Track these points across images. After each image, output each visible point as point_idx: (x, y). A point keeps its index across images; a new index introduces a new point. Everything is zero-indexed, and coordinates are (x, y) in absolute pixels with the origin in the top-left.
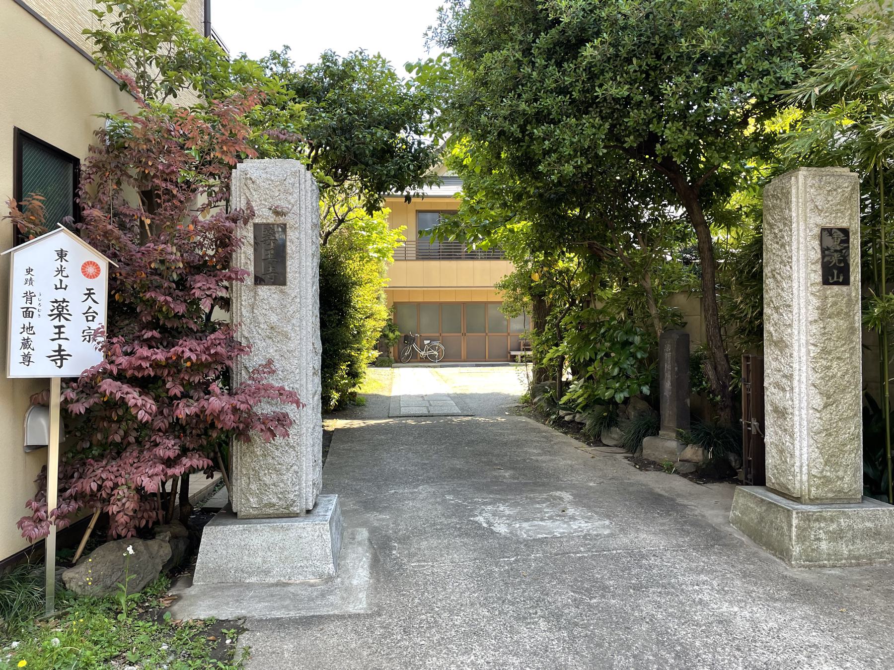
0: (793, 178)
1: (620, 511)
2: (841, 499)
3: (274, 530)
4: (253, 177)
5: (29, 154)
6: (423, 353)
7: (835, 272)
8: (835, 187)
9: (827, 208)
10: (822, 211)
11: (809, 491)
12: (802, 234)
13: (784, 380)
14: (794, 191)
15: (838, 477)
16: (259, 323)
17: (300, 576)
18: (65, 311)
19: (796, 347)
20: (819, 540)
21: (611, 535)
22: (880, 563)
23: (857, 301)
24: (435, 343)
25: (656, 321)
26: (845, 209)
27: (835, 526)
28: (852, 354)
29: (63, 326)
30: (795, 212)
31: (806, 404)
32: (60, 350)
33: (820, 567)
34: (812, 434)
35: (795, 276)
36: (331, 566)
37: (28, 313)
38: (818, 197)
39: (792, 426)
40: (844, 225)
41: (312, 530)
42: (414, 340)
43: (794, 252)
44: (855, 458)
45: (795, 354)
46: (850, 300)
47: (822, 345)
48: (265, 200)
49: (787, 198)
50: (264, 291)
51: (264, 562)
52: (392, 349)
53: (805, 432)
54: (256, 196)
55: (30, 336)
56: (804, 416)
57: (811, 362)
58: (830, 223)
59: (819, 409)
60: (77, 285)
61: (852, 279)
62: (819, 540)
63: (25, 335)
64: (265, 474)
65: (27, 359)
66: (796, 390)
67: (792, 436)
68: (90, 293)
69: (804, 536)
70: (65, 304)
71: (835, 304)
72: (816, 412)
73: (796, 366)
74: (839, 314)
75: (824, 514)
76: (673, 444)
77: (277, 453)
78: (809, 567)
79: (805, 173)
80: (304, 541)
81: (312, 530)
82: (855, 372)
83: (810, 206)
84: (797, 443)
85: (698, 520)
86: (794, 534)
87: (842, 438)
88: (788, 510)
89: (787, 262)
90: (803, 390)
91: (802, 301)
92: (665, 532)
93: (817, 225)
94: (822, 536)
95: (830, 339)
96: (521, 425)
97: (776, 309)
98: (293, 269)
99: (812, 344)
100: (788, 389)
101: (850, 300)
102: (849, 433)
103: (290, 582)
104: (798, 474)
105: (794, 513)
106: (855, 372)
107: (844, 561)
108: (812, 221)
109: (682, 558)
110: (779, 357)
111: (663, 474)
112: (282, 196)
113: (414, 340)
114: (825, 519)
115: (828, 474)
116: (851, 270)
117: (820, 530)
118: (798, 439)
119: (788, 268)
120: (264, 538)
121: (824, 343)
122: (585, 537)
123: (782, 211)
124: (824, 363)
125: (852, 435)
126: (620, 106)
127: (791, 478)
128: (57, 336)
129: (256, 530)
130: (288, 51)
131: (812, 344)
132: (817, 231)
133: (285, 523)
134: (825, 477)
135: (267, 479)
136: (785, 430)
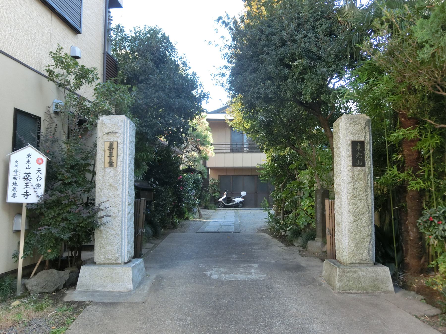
2: (362, 263)
3: (109, 269)
5: (19, 117)
7: (359, 161)
9: (354, 132)
16: (106, 183)
18: (29, 177)
29: (28, 183)
32: (27, 192)
36: (132, 285)
37: (15, 178)
38: (350, 128)
44: (369, 245)
55: (16, 187)
60: (34, 166)
61: (366, 164)
63: (14, 186)
64: (107, 246)
65: (14, 195)
68: (39, 170)
70: (29, 175)
77: (112, 238)
86: (337, 278)
93: (350, 140)
97: (336, 177)
114: (352, 272)
116: (366, 160)
124: (354, 201)
125: (367, 234)
128: (26, 187)
129: (102, 269)
132: (350, 142)
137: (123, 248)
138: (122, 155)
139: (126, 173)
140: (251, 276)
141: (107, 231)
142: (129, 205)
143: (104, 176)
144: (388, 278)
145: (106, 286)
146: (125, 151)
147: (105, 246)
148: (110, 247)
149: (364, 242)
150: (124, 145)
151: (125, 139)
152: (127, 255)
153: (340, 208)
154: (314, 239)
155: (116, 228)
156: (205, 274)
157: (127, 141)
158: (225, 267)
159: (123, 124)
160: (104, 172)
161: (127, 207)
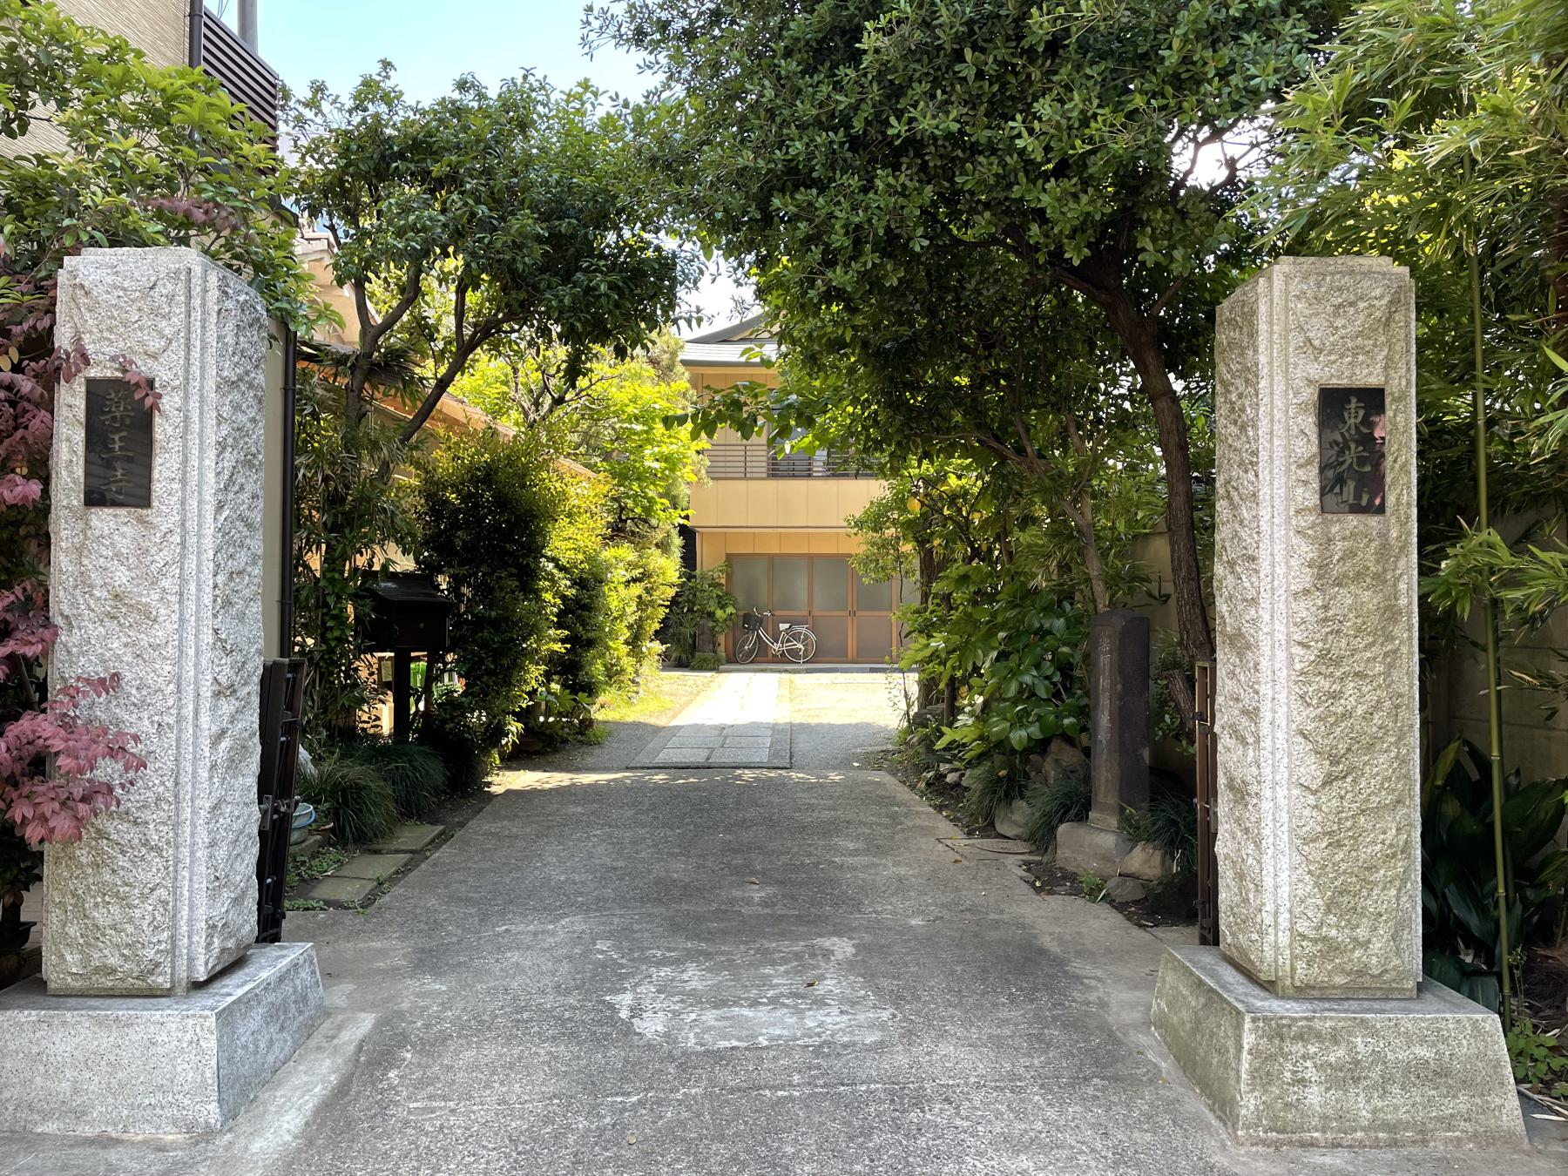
0: (1261, 280)
1: (932, 988)
3: (100, 1024)
4: (86, 284)
6: (776, 647)
8: (1352, 298)
10: (1321, 351)
11: (1293, 969)
12: (1279, 403)
13: (1245, 721)
14: (1263, 309)
15: (1355, 940)
17: (146, 1126)
19: (1265, 648)
20: (1303, 1082)
21: (879, 1047)
22: (1447, 1141)
23: (1403, 548)
24: (798, 629)
25: (1099, 587)
26: (1375, 345)
27: (1341, 1053)
28: (1390, 666)
30: (1264, 356)
31: (1286, 775)
33: (1303, 1144)
34: (1299, 842)
35: (1265, 492)
36: (213, 1107)
38: (1314, 320)
39: (1259, 821)
40: (1374, 380)
41: (178, 1029)
42: (760, 622)
43: (1263, 441)
44: (1398, 898)
45: (1264, 664)
46: (1385, 546)
47: (1320, 645)
48: (110, 330)
49: (1251, 324)
50: (104, 519)
51: (76, 1091)
52: (721, 639)
53: (1285, 837)
54: (90, 322)
56: (1282, 802)
57: (1296, 682)
58: (1339, 378)
59: (1314, 787)
62: (1303, 1082)
64: (96, 905)
66: (1267, 743)
67: (1258, 845)
69: (1268, 1073)
71: (1349, 554)
72: (1307, 794)
73: (1265, 689)
74: (1359, 576)
75: (1317, 1024)
76: (1108, 841)
78: (1277, 1145)
79: (1286, 268)
80: (160, 1050)
81: (178, 1029)
82: (1397, 707)
83: (1296, 339)
84: (1267, 858)
85: (1087, 1014)
86: (1245, 1066)
87: (1366, 852)
88: (1239, 1012)
89: (1250, 465)
90: (1281, 743)
91: (1279, 547)
92: (998, 1043)
94: (1311, 1074)
95: (1338, 631)
96: (866, 788)
97: (1231, 564)
98: (167, 474)
99: (1299, 643)
100: (1251, 740)
101: (1385, 546)
102: (1383, 843)
103: (125, 1136)
104: (1271, 930)
105: (1247, 1018)
106: (1397, 707)
107: (1359, 1135)
108: (1299, 373)
109: (1003, 1108)
110: (1238, 670)
111: (1079, 903)
112: (146, 322)
113: (760, 622)
114: (1319, 1036)
115: (1333, 933)
116: (1388, 479)
117: (1306, 1060)
118: (1270, 852)
119: (1251, 476)
120: (77, 1040)
121: (1325, 641)
122: (818, 1051)
123: (1242, 354)
124: (1326, 684)
125: (1391, 846)
126: (964, 151)
127: (1255, 936)
129: (64, 1023)
130: (392, 73)
131: (1299, 643)
132: (1310, 395)
133: (122, 1010)
134: (1325, 939)
135: (99, 916)
136: (1247, 831)
137: (185, 913)
138: (176, 445)
139: (199, 535)
140: (820, 1015)
141: (98, 831)
142: (217, 695)
143: (80, 550)
144: (1497, 1065)
145: (84, 1113)
146: (196, 427)
147: (89, 904)
148: (115, 909)
149: (1376, 884)
150: (186, 398)
151: (195, 370)
152: (209, 945)
153: (1253, 714)
154: (1082, 817)
155: (144, 815)
156: (612, 1007)
157: (203, 377)
158: (708, 955)
159: (181, 286)
160: (83, 531)
161: (206, 704)
